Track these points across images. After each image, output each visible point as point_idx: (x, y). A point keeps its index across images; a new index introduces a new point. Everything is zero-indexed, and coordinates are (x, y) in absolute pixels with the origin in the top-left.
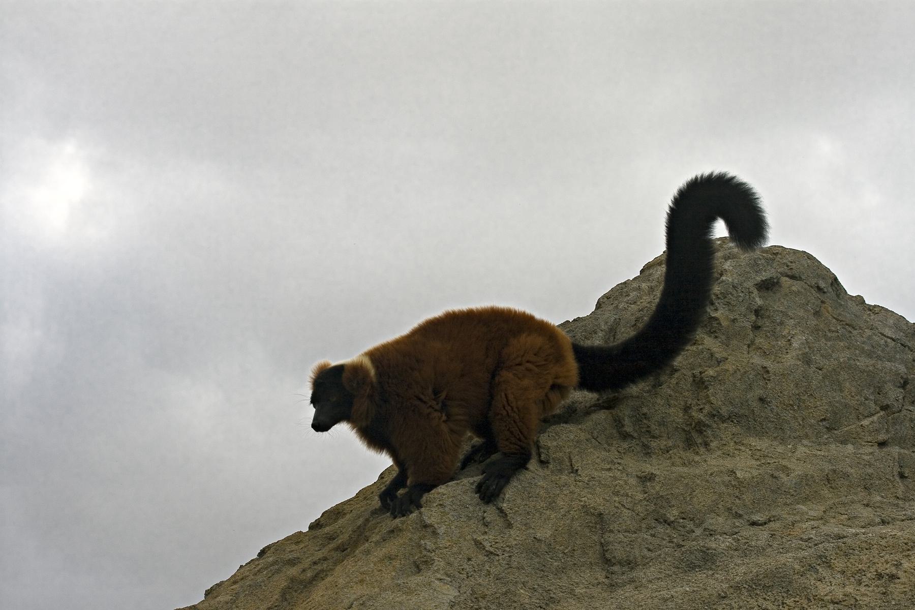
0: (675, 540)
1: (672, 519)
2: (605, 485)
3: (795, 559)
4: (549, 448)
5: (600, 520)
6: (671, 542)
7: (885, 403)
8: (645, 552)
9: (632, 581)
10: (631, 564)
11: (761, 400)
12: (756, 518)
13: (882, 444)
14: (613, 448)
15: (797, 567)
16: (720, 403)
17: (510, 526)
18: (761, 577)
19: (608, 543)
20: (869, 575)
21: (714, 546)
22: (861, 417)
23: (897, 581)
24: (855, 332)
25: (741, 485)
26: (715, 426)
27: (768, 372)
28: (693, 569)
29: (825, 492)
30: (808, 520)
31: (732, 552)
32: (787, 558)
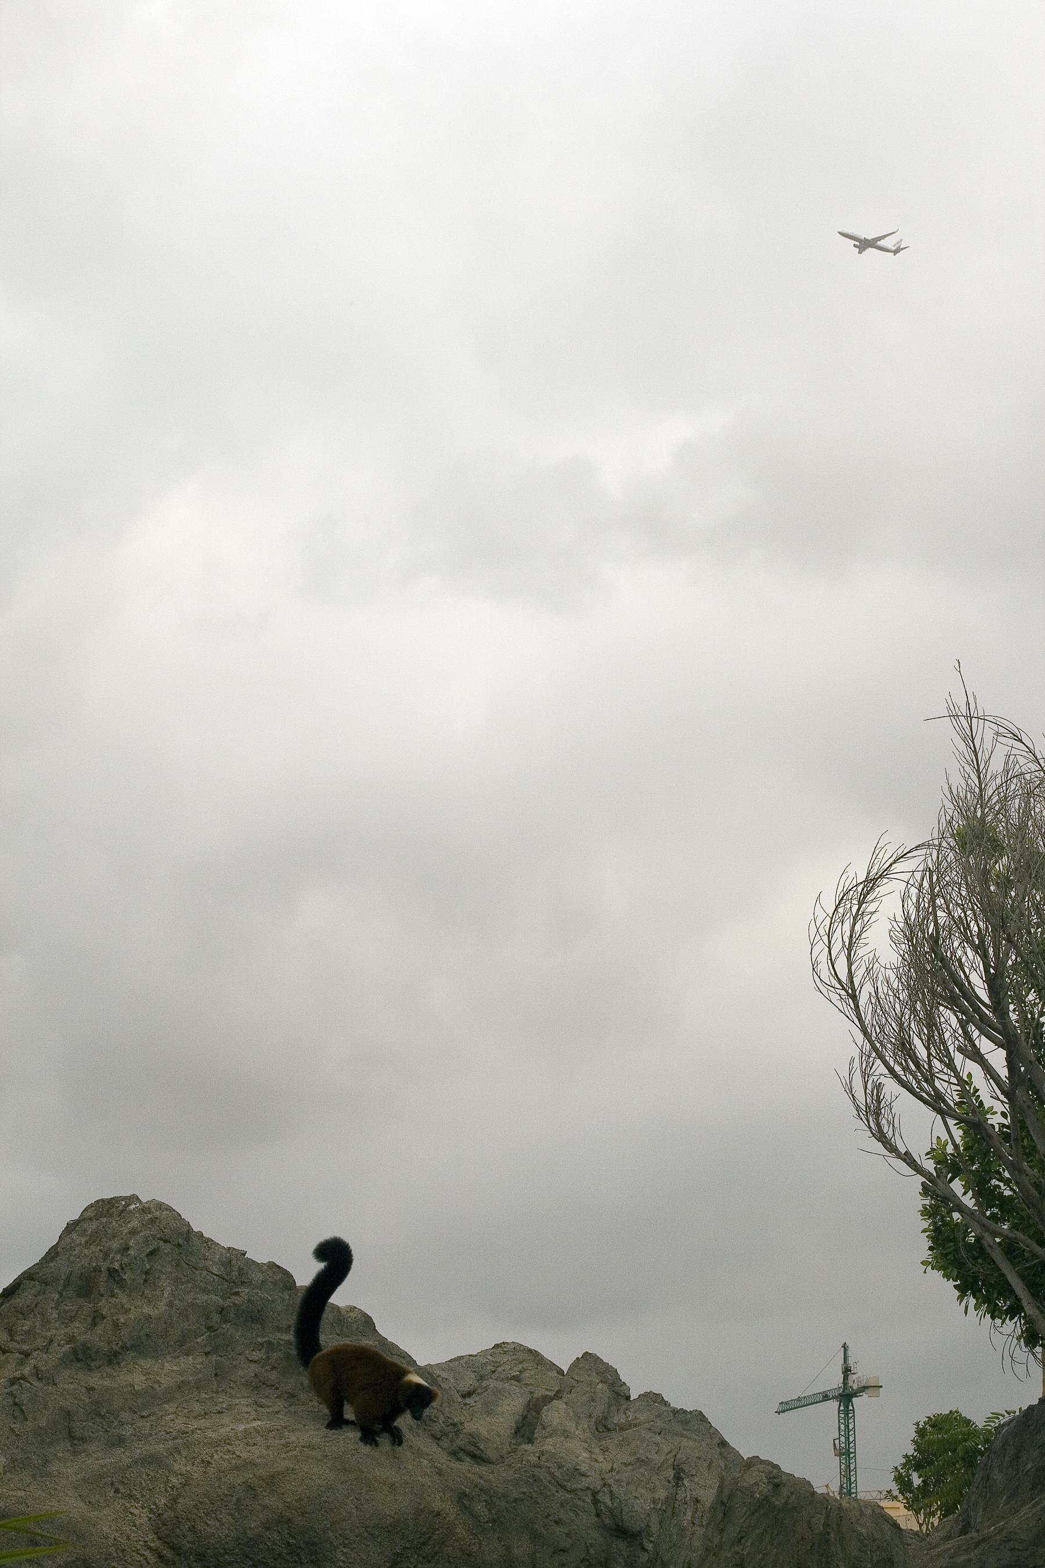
0: (104, 1427)
1: (103, 1414)
2: (70, 1394)
3: (164, 1449)
4: (43, 1371)
5: (68, 1414)
6: (103, 1428)
7: (210, 1325)
8: (90, 1434)
9: (84, 1451)
10: (83, 1440)
11: (147, 1335)
12: (145, 1414)
13: (207, 1354)
14: (72, 1367)
15: (165, 1453)
16: (127, 1340)
17: (26, 1419)
18: (147, 1457)
19: (73, 1428)
20: (198, 1461)
21: (124, 1433)
22: (197, 1337)
23: (211, 1465)
24: (197, 1272)
25: (136, 1394)
26: (123, 1353)
27: (151, 1318)
28: (114, 1445)
29: (178, 1396)
30: (169, 1414)
31: (132, 1437)
32: (160, 1448)
